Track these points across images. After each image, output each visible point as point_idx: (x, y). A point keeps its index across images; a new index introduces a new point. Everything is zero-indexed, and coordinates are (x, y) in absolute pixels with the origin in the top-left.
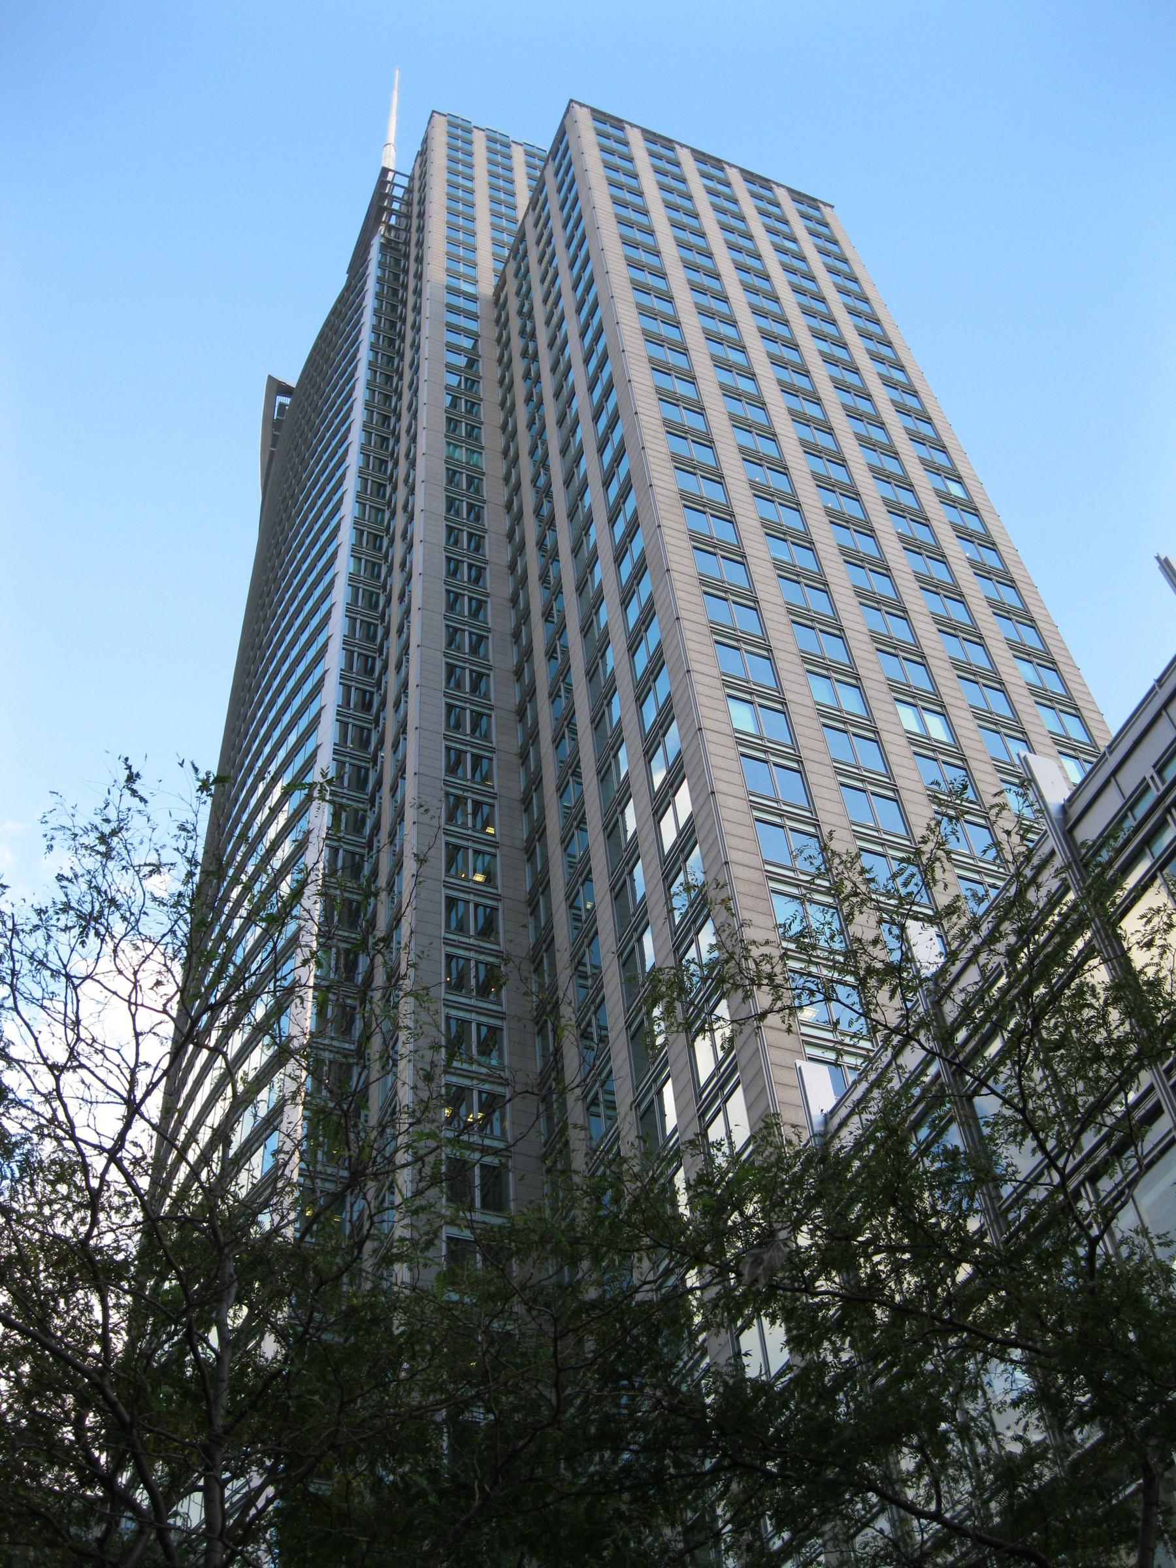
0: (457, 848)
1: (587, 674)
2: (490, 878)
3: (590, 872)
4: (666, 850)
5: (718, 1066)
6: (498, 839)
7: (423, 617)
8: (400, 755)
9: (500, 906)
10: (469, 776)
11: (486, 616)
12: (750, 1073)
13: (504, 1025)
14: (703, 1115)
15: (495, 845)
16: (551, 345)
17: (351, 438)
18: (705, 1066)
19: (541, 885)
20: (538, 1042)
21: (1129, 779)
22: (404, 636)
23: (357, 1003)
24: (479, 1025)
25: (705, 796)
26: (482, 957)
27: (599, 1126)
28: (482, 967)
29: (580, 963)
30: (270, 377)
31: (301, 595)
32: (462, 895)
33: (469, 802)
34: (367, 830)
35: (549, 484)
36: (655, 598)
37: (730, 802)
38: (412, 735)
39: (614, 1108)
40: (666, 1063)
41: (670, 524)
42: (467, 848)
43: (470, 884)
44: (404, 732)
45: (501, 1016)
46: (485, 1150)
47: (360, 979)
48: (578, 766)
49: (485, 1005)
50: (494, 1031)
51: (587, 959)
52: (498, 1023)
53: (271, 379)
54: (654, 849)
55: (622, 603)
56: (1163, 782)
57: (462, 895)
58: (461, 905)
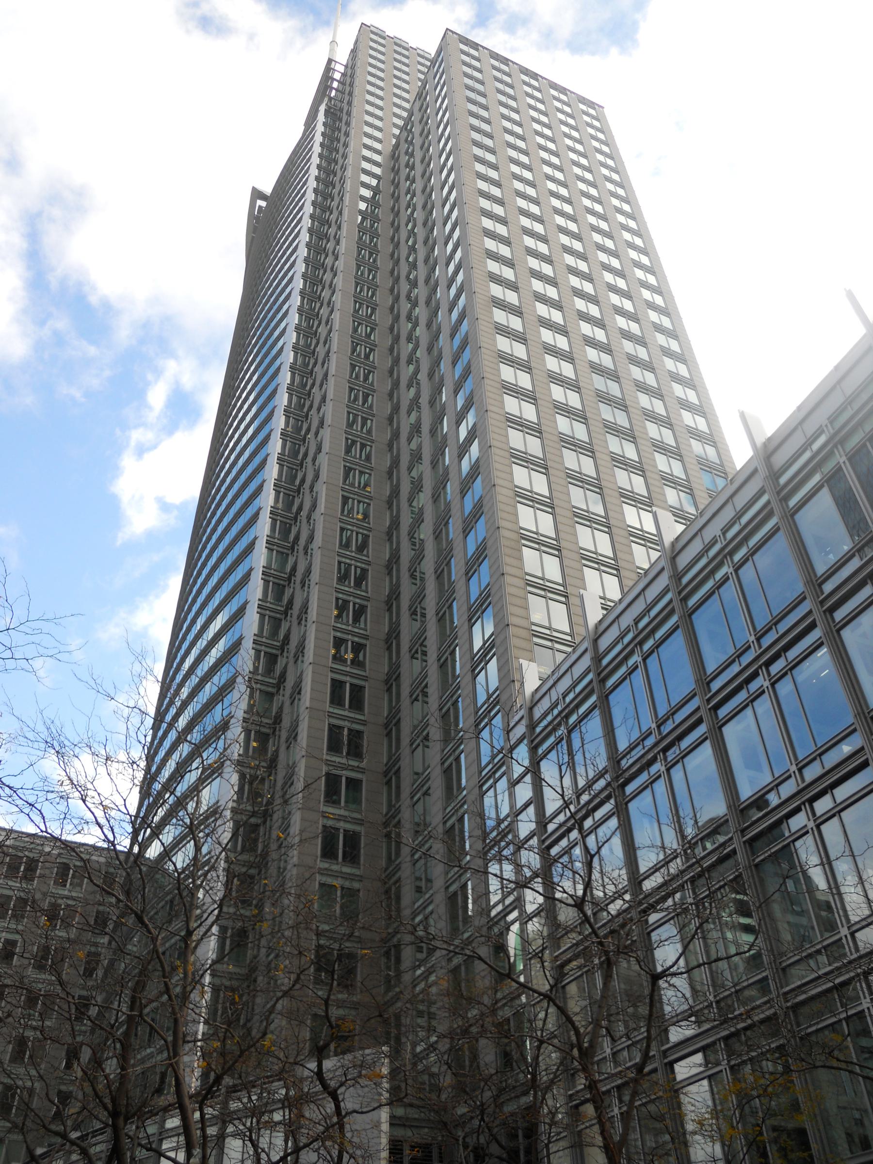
0: (350, 469)
1: (430, 403)
2: (366, 516)
3: (422, 487)
4: (466, 515)
5: (485, 643)
6: (372, 494)
7: (335, 381)
8: (319, 438)
9: (370, 568)
10: (359, 429)
11: (368, 552)
12: (501, 650)
13: (366, 684)
14: (474, 670)
15: (370, 498)
16: (422, 161)
17: (303, 222)
18: (478, 644)
19: (395, 523)
20: (385, 789)
21: (709, 534)
22: (327, 346)
23: (290, 552)
24: (356, 567)
25: (486, 448)
26: (359, 564)
27: (417, 664)
28: (360, 536)
29: (412, 537)
30: (253, 188)
31: (272, 300)
32: (352, 496)
33: (348, 685)
34: (300, 457)
35: (416, 260)
36: (472, 363)
37: (498, 451)
38: (331, 381)
39: (427, 696)
40: (459, 688)
41: (483, 317)
42: (355, 470)
43: (355, 521)
44: (325, 402)
45: (367, 599)
46: (354, 634)
47: (281, 636)
48: (420, 427)
49: (359, 592)
50: (364, 571)
51: (418, 570)
52: (366, 567)
53: (254, 189)
54: (464, 598)
55: (453, 363)
56: (725, 540)
57: (352, 496)
58: (350, 500)
